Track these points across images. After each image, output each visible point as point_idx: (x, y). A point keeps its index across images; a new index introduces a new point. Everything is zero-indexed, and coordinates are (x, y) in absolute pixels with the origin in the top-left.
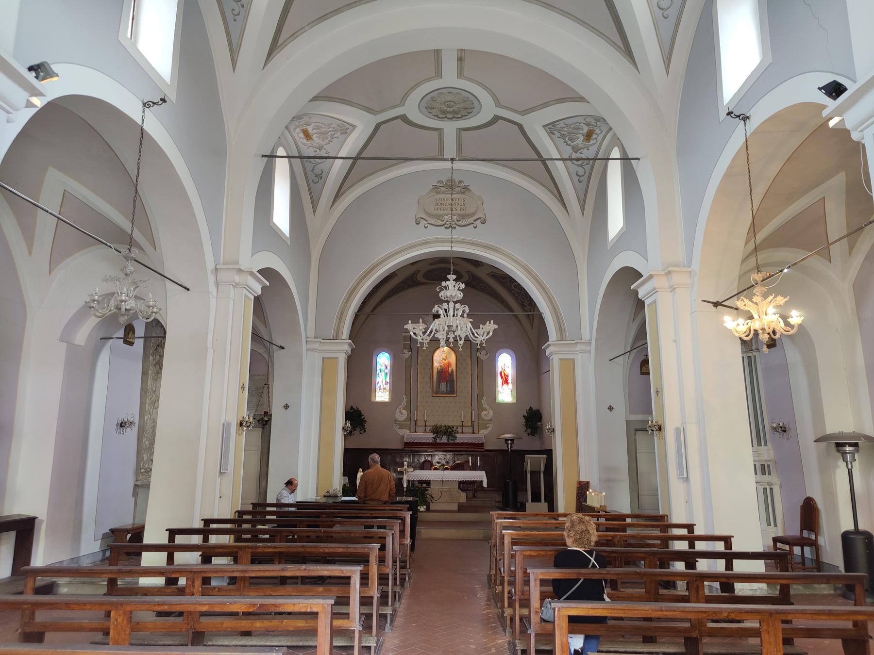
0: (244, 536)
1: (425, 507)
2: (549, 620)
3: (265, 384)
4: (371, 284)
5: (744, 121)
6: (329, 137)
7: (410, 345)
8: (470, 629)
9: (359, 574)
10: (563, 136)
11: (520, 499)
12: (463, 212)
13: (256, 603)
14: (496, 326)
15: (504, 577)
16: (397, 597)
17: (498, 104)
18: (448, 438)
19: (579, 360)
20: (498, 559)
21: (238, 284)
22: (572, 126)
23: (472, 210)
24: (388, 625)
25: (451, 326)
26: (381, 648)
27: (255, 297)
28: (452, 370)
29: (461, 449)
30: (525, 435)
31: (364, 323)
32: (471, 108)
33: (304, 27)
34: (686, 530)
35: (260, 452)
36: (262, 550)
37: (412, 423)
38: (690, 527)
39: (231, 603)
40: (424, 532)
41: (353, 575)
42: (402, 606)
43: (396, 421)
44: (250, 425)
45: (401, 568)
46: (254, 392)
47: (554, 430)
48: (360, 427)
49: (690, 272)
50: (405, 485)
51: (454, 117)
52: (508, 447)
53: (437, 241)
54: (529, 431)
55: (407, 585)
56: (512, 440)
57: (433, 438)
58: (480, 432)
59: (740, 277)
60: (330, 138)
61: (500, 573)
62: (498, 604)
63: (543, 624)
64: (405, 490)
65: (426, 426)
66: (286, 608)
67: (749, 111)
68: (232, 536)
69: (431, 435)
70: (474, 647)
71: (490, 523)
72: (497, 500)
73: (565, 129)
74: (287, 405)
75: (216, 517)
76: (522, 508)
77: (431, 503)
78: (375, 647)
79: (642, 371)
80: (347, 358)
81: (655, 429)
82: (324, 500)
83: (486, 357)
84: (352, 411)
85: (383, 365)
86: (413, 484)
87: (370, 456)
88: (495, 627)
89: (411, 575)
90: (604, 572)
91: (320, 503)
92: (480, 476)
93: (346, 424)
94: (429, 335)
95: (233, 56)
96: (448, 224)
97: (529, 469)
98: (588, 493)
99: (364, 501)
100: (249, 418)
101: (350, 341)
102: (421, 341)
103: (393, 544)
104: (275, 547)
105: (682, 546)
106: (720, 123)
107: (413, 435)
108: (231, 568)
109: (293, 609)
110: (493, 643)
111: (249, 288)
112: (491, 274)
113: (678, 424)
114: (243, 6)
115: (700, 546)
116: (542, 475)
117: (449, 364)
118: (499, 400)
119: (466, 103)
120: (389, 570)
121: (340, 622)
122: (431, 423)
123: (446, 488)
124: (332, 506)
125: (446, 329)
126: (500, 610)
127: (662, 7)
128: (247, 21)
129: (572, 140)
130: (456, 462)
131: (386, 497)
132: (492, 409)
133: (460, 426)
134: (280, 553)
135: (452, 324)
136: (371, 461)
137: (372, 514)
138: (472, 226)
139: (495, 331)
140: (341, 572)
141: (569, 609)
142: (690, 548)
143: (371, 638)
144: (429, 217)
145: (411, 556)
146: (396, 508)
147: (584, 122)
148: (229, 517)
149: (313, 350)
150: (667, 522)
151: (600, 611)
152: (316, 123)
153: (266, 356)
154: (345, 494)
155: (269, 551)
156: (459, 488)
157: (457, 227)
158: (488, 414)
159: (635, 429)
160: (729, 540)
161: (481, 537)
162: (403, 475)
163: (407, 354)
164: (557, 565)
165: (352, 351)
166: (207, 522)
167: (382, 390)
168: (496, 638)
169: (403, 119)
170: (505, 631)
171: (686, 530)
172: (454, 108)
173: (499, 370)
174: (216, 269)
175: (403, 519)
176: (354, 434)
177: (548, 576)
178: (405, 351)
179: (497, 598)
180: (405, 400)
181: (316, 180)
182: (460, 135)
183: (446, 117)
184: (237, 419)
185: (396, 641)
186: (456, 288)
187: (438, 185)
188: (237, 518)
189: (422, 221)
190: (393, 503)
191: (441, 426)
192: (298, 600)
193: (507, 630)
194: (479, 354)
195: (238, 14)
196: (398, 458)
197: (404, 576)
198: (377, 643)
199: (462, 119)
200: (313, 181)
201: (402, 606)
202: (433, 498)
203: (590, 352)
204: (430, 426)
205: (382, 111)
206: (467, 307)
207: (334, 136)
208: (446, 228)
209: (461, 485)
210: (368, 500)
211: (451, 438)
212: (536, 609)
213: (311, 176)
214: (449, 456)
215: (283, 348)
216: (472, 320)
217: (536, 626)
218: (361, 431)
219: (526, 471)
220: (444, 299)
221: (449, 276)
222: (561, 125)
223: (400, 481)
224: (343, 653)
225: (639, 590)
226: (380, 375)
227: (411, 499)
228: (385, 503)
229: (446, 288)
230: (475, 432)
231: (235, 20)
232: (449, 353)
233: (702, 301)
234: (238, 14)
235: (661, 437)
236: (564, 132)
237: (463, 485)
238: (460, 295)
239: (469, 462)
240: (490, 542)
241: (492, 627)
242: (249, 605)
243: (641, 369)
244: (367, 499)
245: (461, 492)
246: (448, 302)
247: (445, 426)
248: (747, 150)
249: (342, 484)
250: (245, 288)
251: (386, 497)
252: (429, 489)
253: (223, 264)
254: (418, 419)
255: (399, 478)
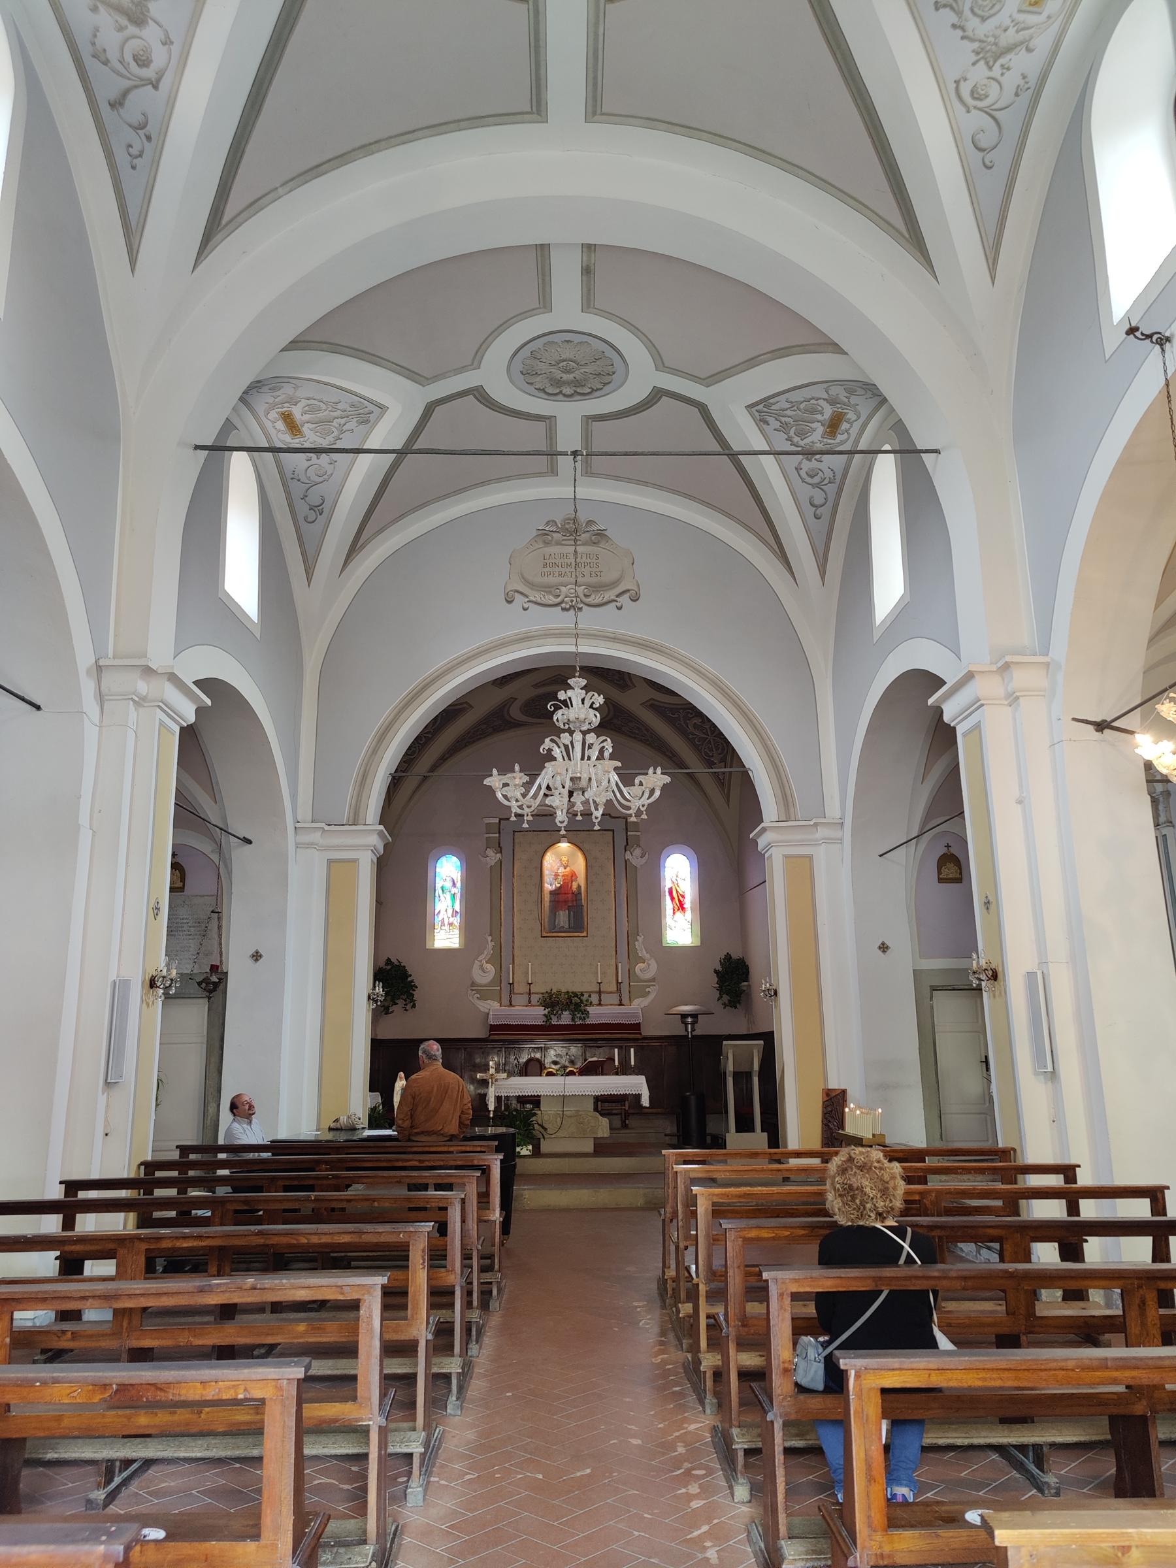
0: (157, 1214)
1: (530, 1147)
2: (811, 1386)
3: (212, 912)
4: (417, 721)
5: (1161, 345)
6: (334, 429)
7: (499, 840)
8: (627, 1400)
9: (378, 1293)
10: (784, 427)
11: (712, 1127)
12: (594, 580)
13: (108, 1382)
14: (667, 779)
15: (698, 1285)
16: (474, 1333)
17: (661, 365)
18: (574, 1015)
19: (821, 856)
20: (682, 1246)
21: (144, 699)
22: (802, 406)
23: (614, 575)
24: (453, 1398)
25: (576, 778)
26: (437, 1452)
27: (182, 729)
28: (579, 887)
29: (598, 1036)
30: (717, 1007)
31: (411, 798)
32: (608, 374)
33: (277, 188)
34: (1061, 1177)
35: (205, 1046)
36: (170, 1245)
37: (505, 989)
38: (1069, 1172)
39: (44, 1383)
40: (529, 1196)
41: (366, 1297)
42: (483, 1353)
43: (473, 984)
44: (170, 985)
45: (484, 1269)
46: (192, 929)
47: (776, 993)
48: (405, 997)
49: (1048, 664)
50: (491, 1107)
51: (575, 391)
52: (687, 1030)
53: (546, 635)
54: (726, 998)
55: (494, 1305)
56: (695, 1016)
57: (544, 1015)
58: (634, 1003)
59: (1144, 673)
60: (336, 433)
61: (687, 1274)
62: (684, 1341)
63: (802, 1397)
64: (491, 1116)
65: (530, 994)
66: (183, 1392)
67: (1170, 326)
68: (132, 1216)
69: (541, 1011)
70: (639, 1442)
71: (661, 1174)
72: (668, 1132)
73: (789, 413)
74: (257, 952)
75: (95, 1175)
76: (718, 1142)
77: (542, 1140)
78: (421, 1454)
79: (941, 876)
80: (375, 861)
81: (984, 977)
82: (329, 1136)
83: (643, 861)
84: (389, 967)
85: (448, 879)
86: (507, 1106)
87: (422, 1046)
88: (681, 1395)
89: (503, 1284)
90: (936, 1274)
91: (321, 1141)
92: (637, 1085)
93: (374, 987)
94: (535, 797)
95: (130, 241)
96: (566, 603)
97: (730, 1068)
98: (847, 1110)
99: (410, 1135)
100: (168, 970)
101: (382, 827)
102: (519, 811)
103: (463, 1221)
104: (200, 1237)
105: (1051, 1210)
106: (1106, 362)
107: (506, 1010)
108: (80, 1291)
109: (202, 1395)
110: (678, 1431)
111: (165, 707)
112: (648, 704)
113: (1031, 965)
114: (149, 138)
115: (1090, 1210)
116: (756, 1080)
117: (573, 876)
118: (668, 942)
119: (598, 363)
120: (454, 1277)
121: (334, 1410)
122: (540, 988)
123: (570, 1109)
124: (342, 1147)
125: (568, 784)
126: (689, 1356)
127: (983, 145)
128: (157, 170)
129: (802, 434)
130: (590, 1060)
131: (453, 1128)
132: (655, 959)
133: (596, 992)
134: (221, 1249)
135: (579, 775)
136: (424, 1056)
137: (423, 1161)
138: (613, 605)
139: (665, 788)
140: (339, 1289)
141: (883, 1372)
142: (1154, 1212)
143: (413, 1435)
144: (532, 589)
145: (502, 1244)
146: (471, 1149)
147: (826, 396)
148: (124, 1175)
149: (309, 846)
150: (1015, 1162)
151: (958, 1375)
152: (308, 399)
153: (215, 857)
154: (374, 1122)
155: (185, 1245)
156: (596, 1109)
157: (585, 608)
158: (647, 969)
159: (930, 986)
160: (1159, 1195)
161: (640, 1202)
162: (487, 1087)
163: (493, 857)
164: (827, 1259)
165: (385, 847)
166: (72, 1187)
167: (446, 927)
168: (685, 1420)
169: (477, 395)
170: (702, 1402)
171: (1061, 1177)
172: (577, 375)
173: (667, 884)
174: (99, 669)
175: (485, 1171)
176: (392, 1012)
177: (810, 1286)
178: (490, 852)
179: (685, 1330)
180: (491, 945)
181: (312, 516)
182: (587, 430)
183: (561, 392)
184: (144, 971)
185: (470, 1435)
186: (588, 703)
187: (547, 529)
188: (142, 1175)
189: (517, 596)
190: (466, 1139)
191: (559, 993)
192: (213, 1372)
193: (707, 1401)
194: (628, 856)
195: (140, 156)
196: (477, 1056)
197: (490, 1286)
198: (427, 1444)
199: (591, 397)
200: (306, 519)
201: (485, 1352)
202: (545, 1129)
203: (841, 840)
204: (537, 993)
205: (436, 378)
206: (609, 740)
207: (345, 428)
208: (564, 609)
209: (599, 1103)
210: (417, 1134)
211: (578, 1015)
212: (783, 1362)
213: (302, 509)
214: (575, 1050)
215: (249, 842)
216: (619, 764)
217: (785, 1403)
218: (406, 1005)
219: (725, 1073)
220: (562, 727)
221: (571, 681)
222: (782, 403)
223: (483, 1097)
224: (353, 1468)
225: (988, 1306)
226: (442, 898)
227: (502, 1130)
228: (452, 1138)
229: (566, 704)
230: (623, 1002)
231: (133, 168)
232: (571, 855)
233: (1075, 719)
234: (140, 156)
235: (997, 993)
236: (787, 419)
237: (605, 1104)
238: (594, 719)
239: (614, 1060)
240: (663, 1213)
241: (675, 1392)
242: (91, 1387)
243: (939, 872)
244: (416, 1131)
245: (600, 1117)
246: (571, 732)
247: (568, 992)
248: (1169, 402)
249: (369, 1106)
250: (159, 706)
251: (453, 1128)
252: (539, 1112)
253: (114, 658)
254: (516, 979)
255: (480, 1094)
